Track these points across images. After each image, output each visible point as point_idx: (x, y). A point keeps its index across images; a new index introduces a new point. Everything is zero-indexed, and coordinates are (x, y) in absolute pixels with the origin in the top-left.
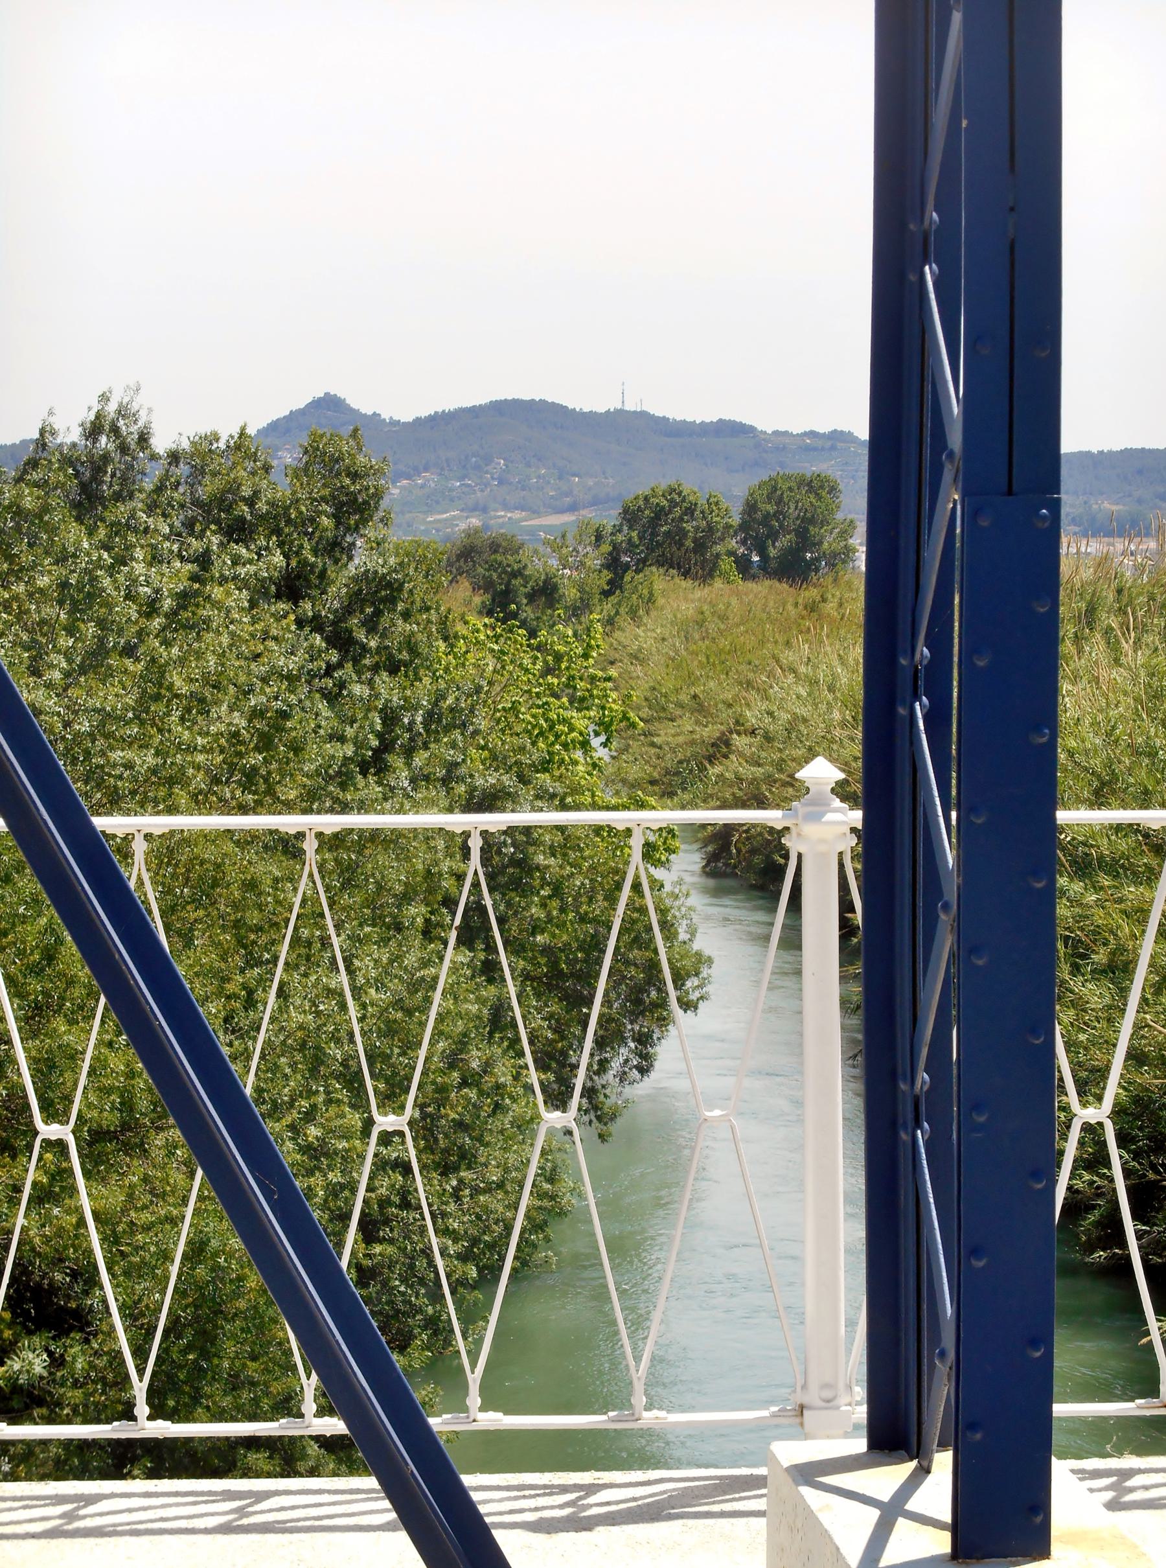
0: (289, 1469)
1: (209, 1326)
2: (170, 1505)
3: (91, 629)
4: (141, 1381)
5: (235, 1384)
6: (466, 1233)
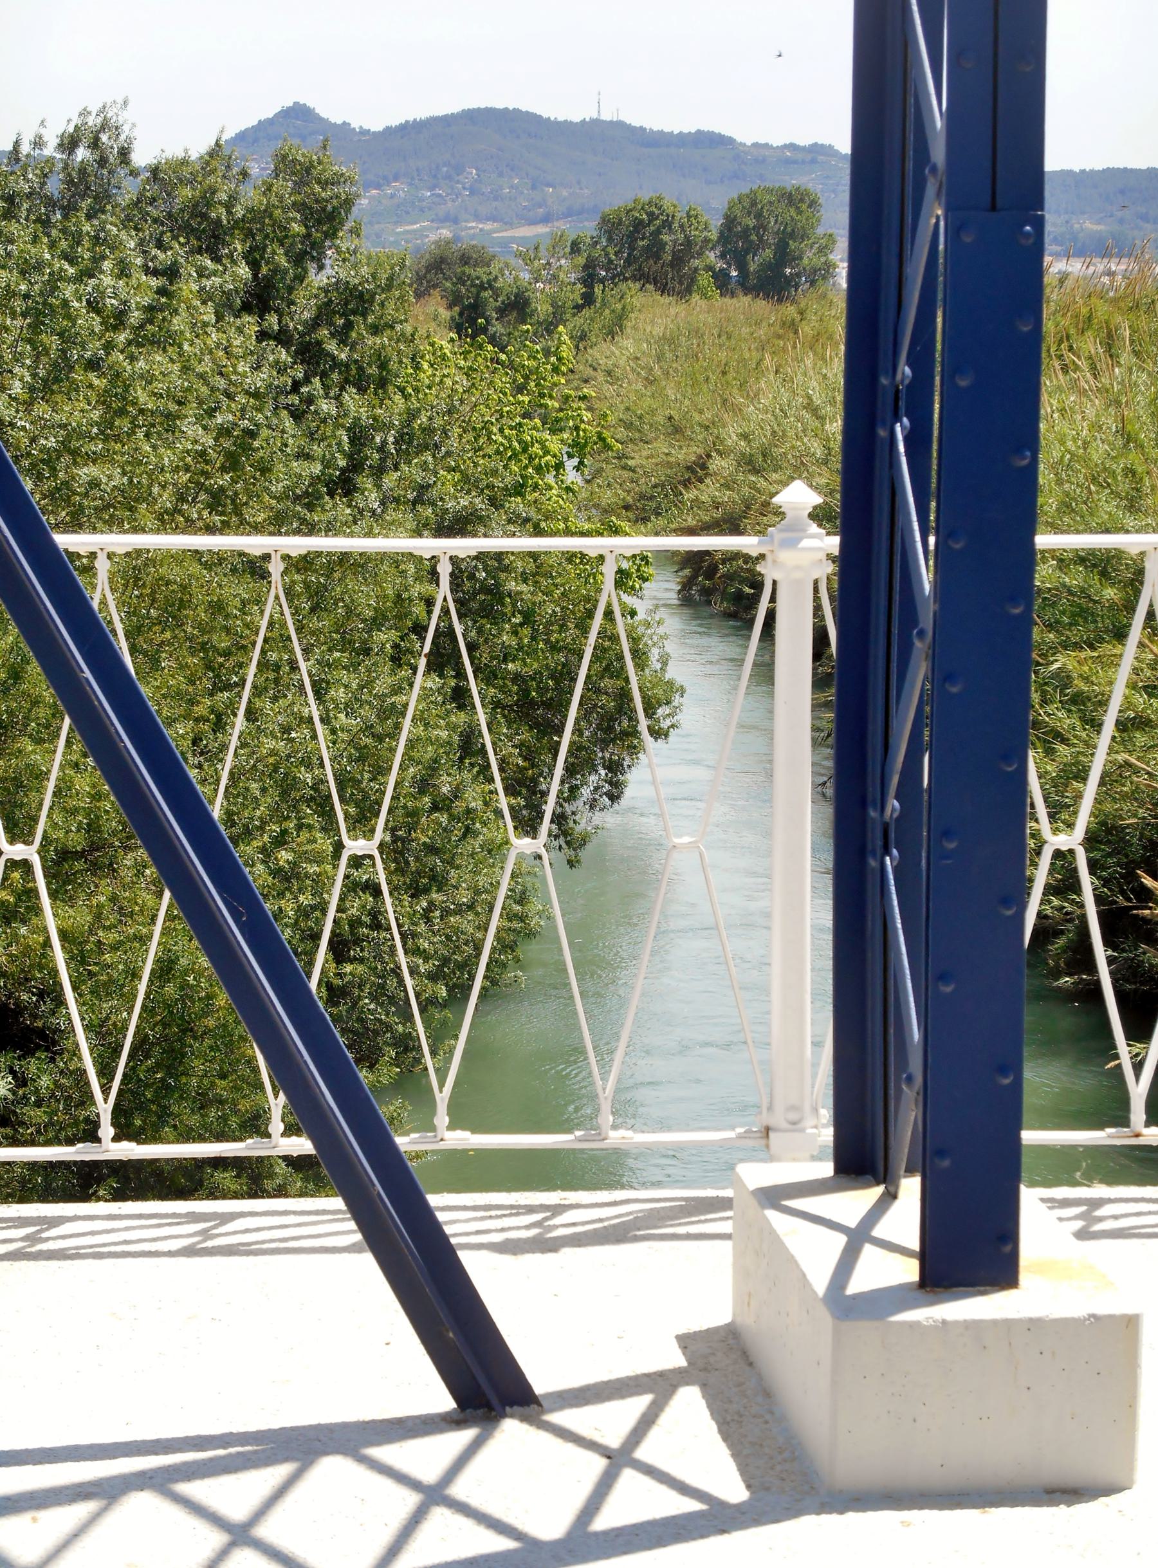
0: (255, 1191)
1: (177, 1045)
2: (134, 1228)
3: (53, 342)
4: (106, 1101)
5: (203, 1102)
6: (436, 952)
